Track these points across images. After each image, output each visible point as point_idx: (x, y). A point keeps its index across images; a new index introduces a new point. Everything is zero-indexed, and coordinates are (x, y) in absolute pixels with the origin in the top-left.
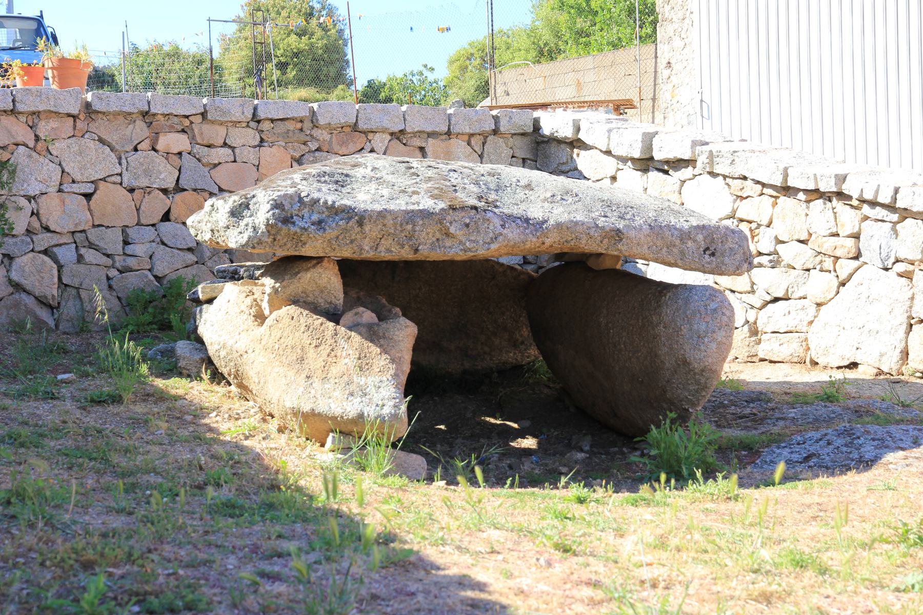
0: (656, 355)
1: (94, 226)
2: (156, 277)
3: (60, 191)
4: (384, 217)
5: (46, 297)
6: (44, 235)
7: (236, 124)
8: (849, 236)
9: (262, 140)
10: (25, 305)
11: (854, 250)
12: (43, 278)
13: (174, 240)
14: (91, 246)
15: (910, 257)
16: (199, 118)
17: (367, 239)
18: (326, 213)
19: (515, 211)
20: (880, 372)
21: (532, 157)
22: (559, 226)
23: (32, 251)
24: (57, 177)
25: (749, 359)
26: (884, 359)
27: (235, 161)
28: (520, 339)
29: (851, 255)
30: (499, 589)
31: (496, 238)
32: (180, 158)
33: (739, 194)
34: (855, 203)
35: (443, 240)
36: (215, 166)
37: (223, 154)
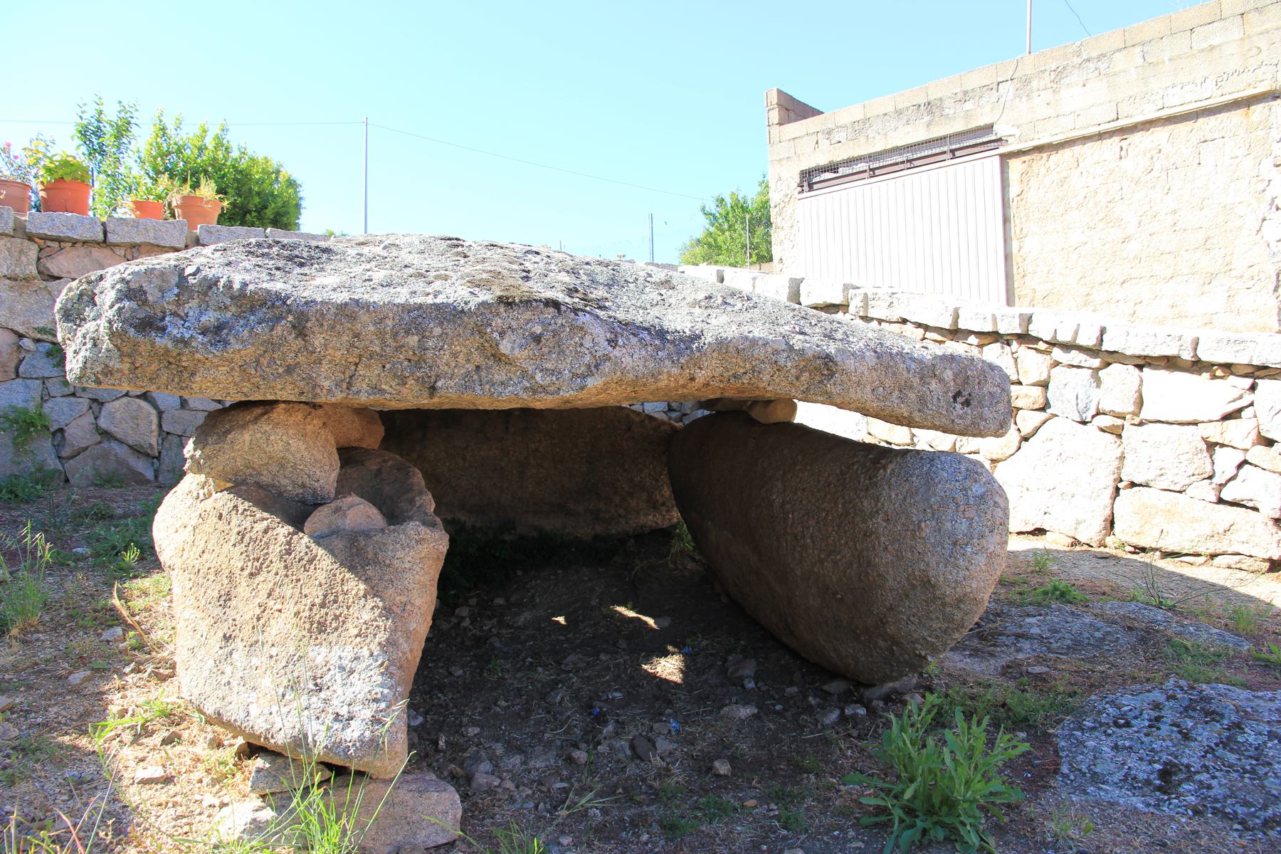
0: (869, 563)
4: (353, 317)
8: (1034, 385)
10: (116, 455)
15: (1119, 409)
17: (325, 366)
18: (233, 309)
19: (639, 318)
20: (1076, 542)
22: (722, 345)
26: (1082, 527)
28: (661, 500)
31: (597, 366)
34: (1042, 346)
35: (488, 368)
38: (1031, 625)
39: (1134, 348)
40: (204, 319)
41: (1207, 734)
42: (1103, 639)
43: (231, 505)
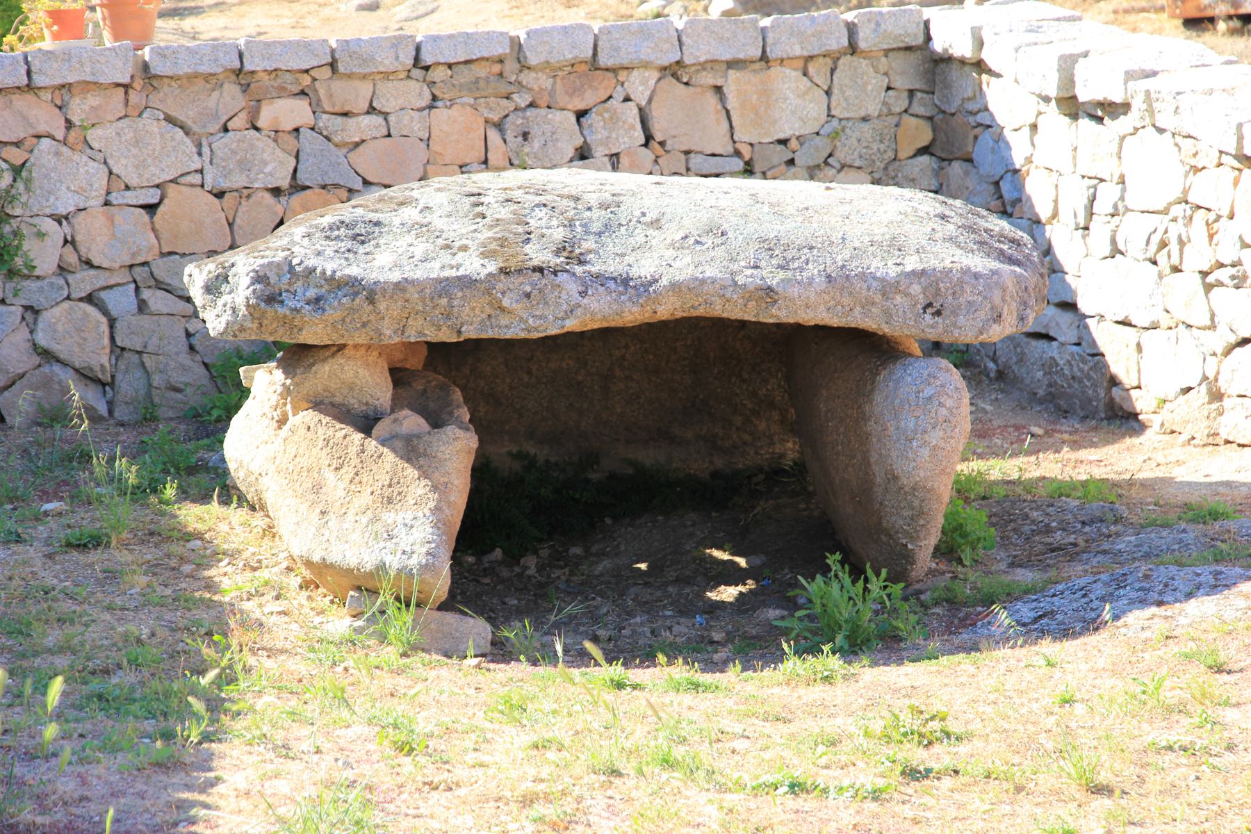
1: (162, 255)
3: (107, 203)
4: (404, 290)
5: (91, 369)
6: (85, 273)
7: (387, 75)
9: (434, 98)
12: (85, 339)
14: (160, 285)
16: (327, 72)
19: (613, 267)
21: (924, 87)
22: (675, 287)
23: (68, 298)
24: (101, 182)
25: (1211, 440)
27: (389, 135)
31: (572, 311)
32: (297, 138)
33: (1193, 162)
35: (496, 316)
37: (368, 125)
40: (308, 294)
43: (317, 419)
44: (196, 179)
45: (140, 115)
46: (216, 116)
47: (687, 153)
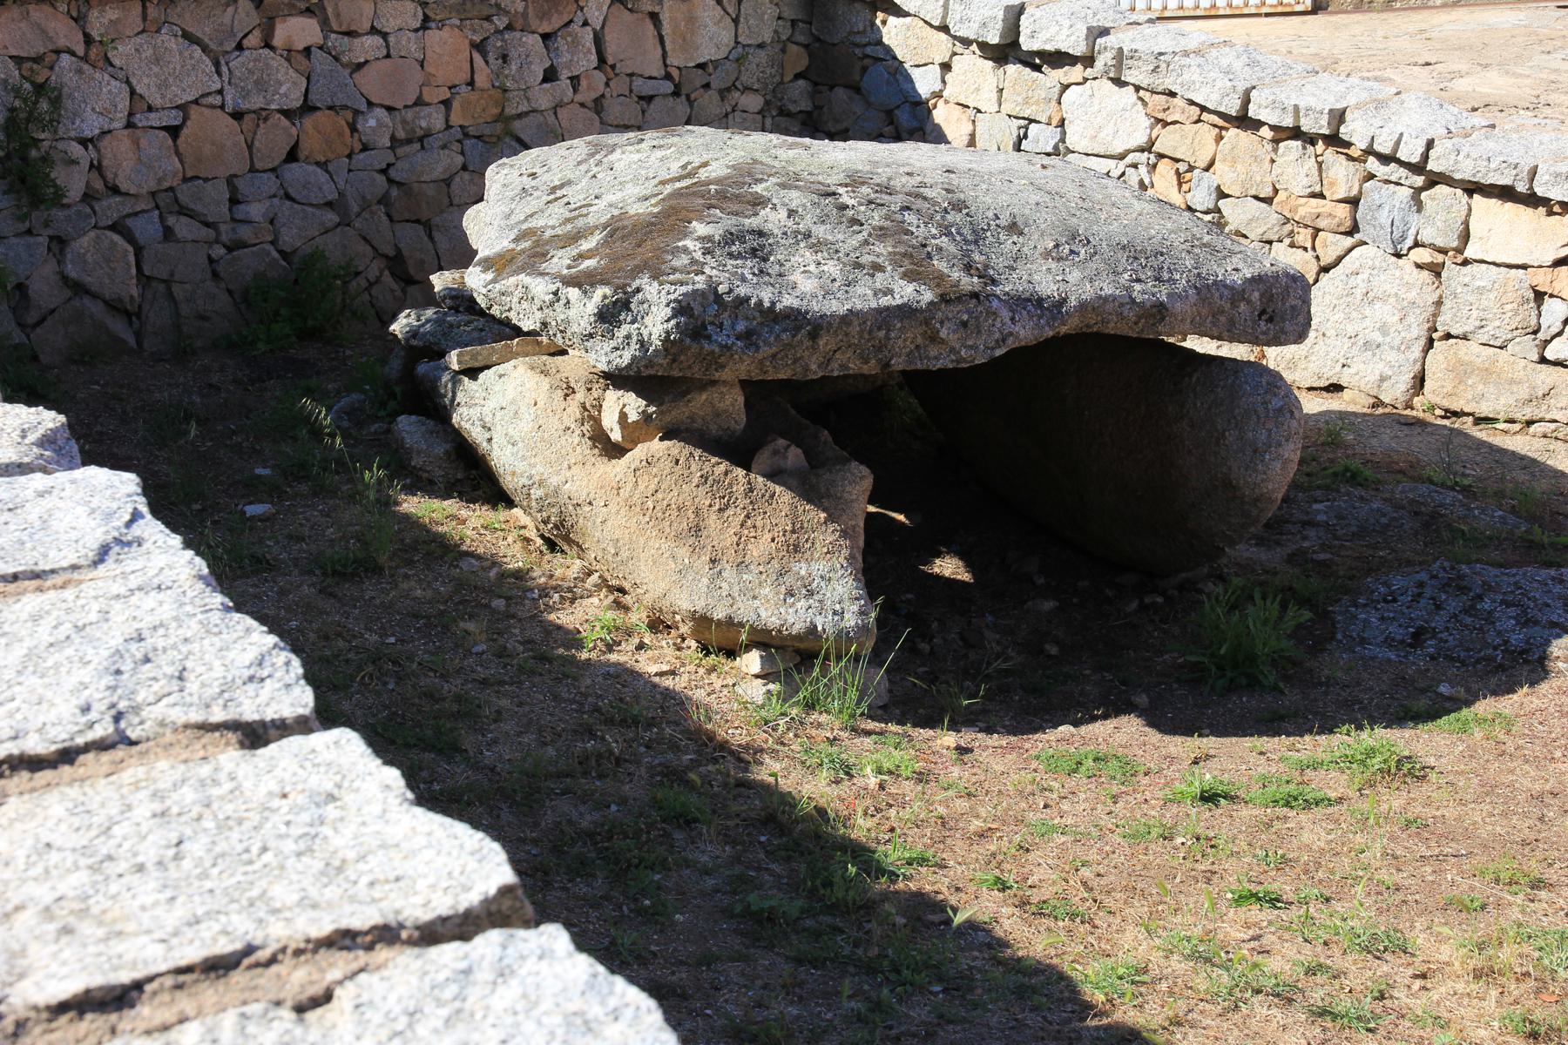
1: (185, 180)
2: (281, 252)
9: (426, 19)
11: (1348, 223)
13: (305, 192)
14: (183, 211)
15: (1440, 242)
20: (1378, 403)
24: (124, 104)
27: (388, 56)
29: (1342, 229)
30: (1106, 961)
33: (1160, 116)
36: (360, 66)
37: (369, 46)
38: (1319, 511)
39: (1464, 172)
41: (1453, 604)
42: (1388, 525)
44: (217, 100)
45: (158, 31)
46: (232, 33)
47: (631, 75)
